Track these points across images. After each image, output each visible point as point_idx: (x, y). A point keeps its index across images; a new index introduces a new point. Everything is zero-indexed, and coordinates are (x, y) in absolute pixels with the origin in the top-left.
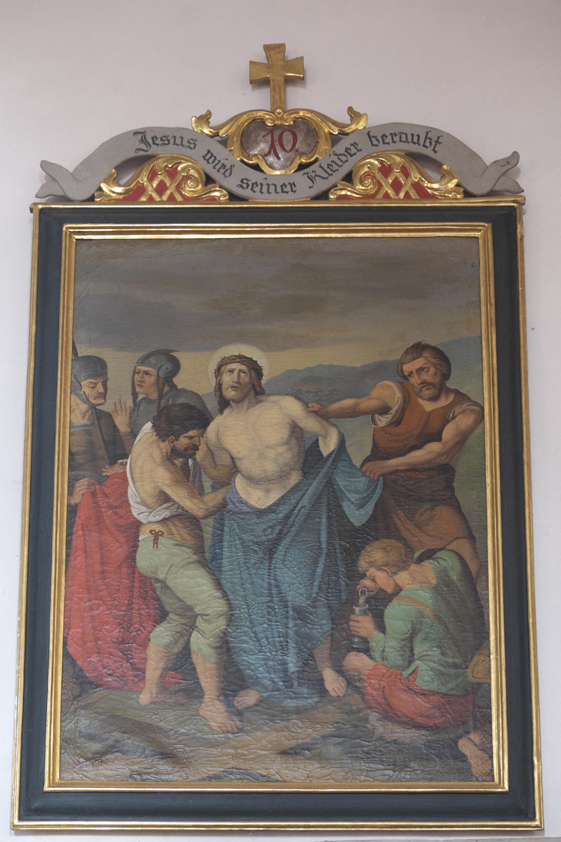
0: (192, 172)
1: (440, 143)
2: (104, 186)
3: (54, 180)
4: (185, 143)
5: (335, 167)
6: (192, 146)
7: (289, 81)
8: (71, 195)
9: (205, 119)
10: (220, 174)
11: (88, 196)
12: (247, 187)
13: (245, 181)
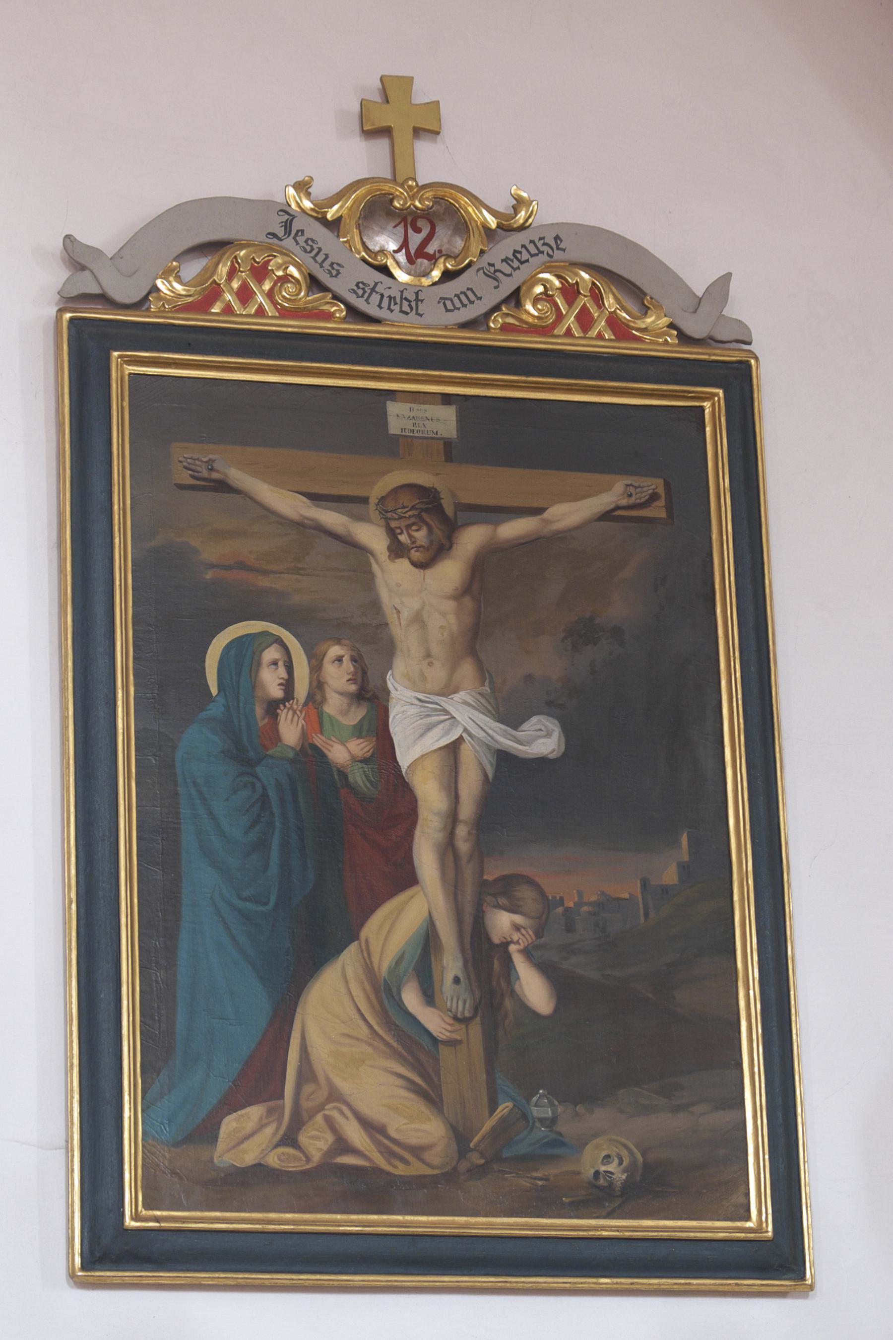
0: (293, 270)
1: (422, 301)
2: (159, 283)
3: (83, 268)
4: (326, 265)
5: (525, 256)
6: (334, 272)
7: (417, 132)
8: (119, 296)
9: (303, 187)
10: (362, 300)
11: (136, 297)
12: (310, 252)
13: (361, 286)
